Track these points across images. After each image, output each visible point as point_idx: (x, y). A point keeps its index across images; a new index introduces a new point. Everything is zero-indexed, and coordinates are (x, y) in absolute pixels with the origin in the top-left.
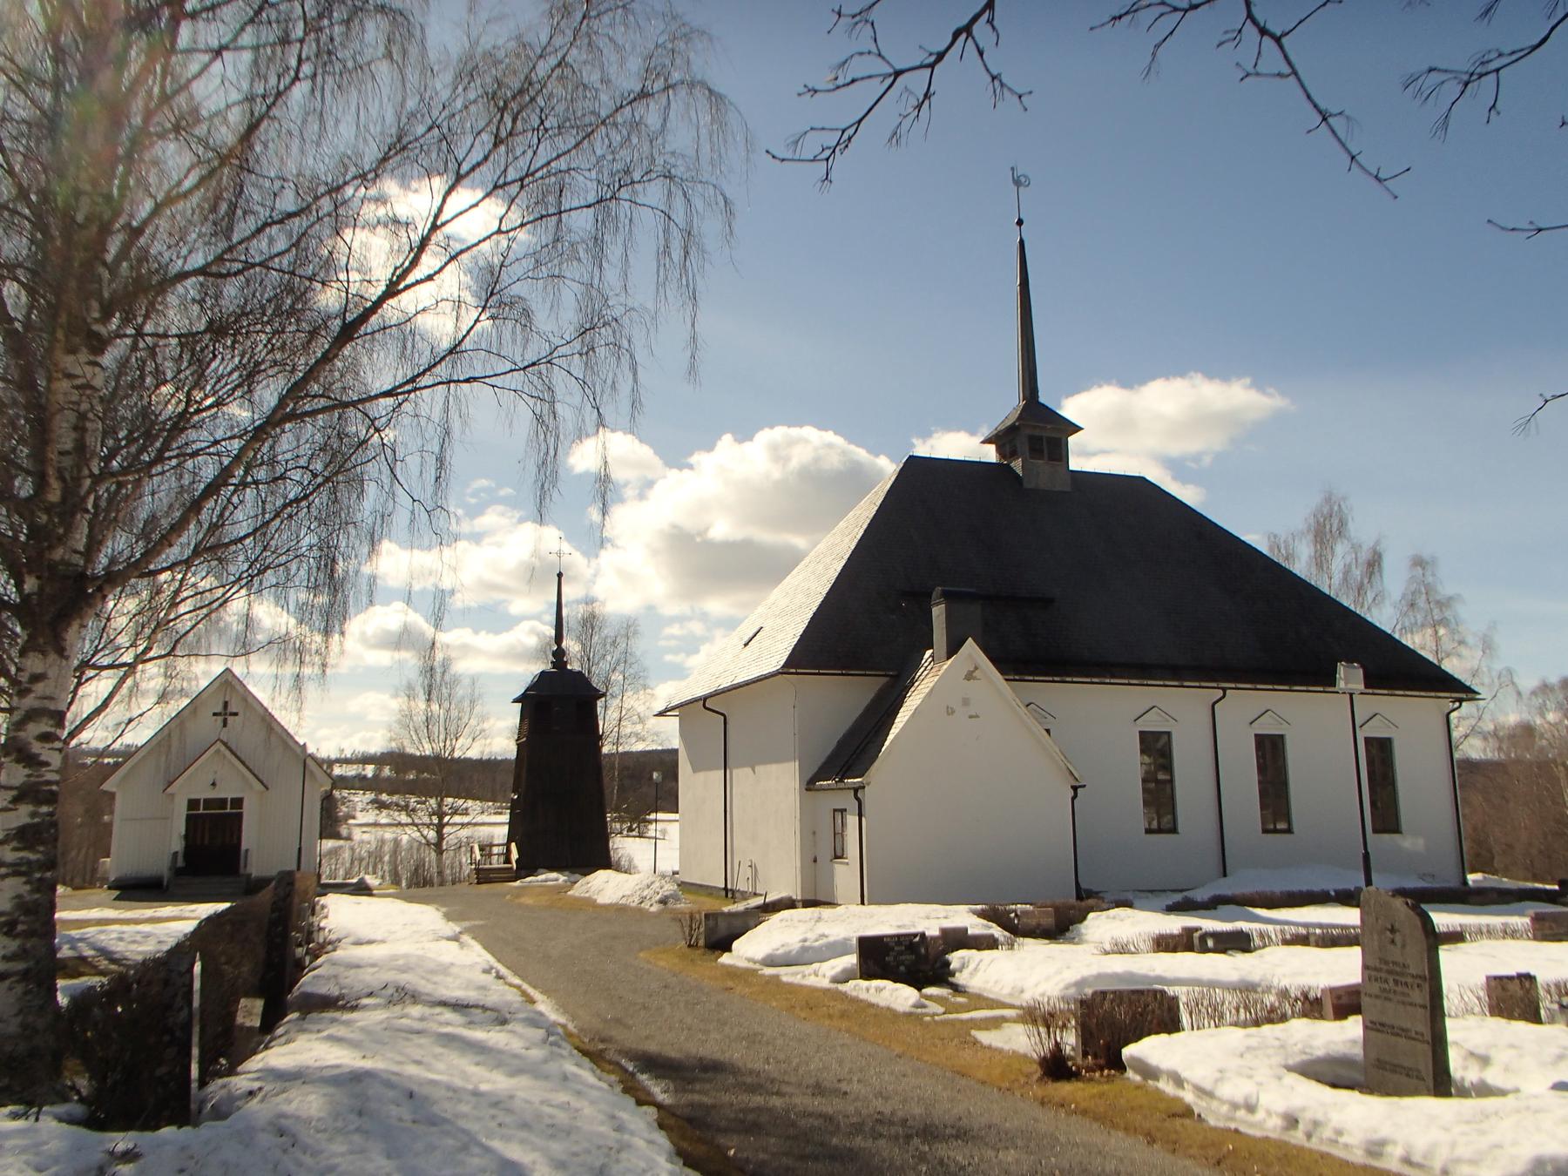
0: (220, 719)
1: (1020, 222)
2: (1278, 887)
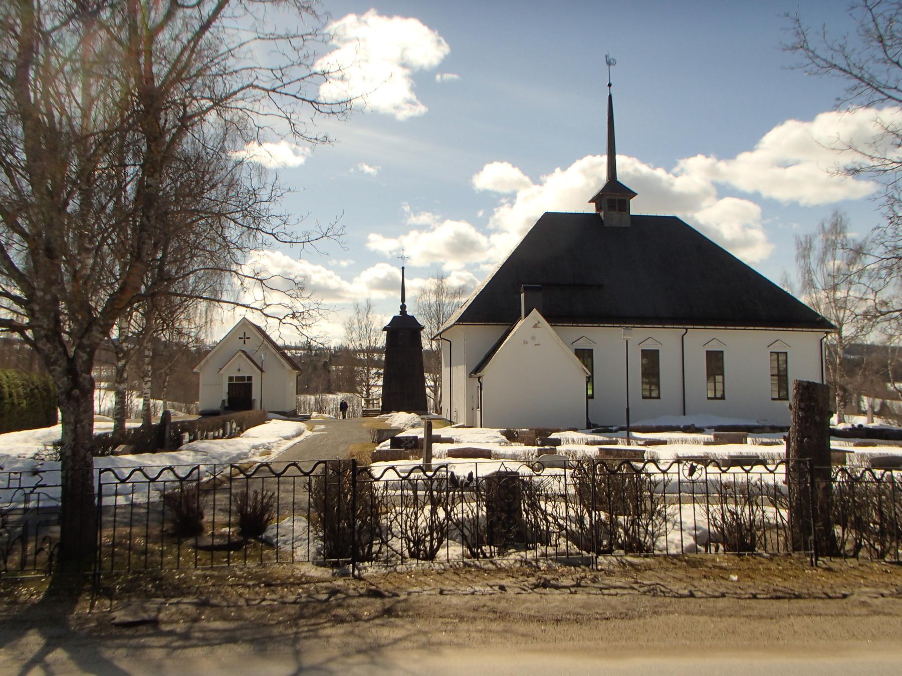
1: (610, 85)
2: (654, 424)
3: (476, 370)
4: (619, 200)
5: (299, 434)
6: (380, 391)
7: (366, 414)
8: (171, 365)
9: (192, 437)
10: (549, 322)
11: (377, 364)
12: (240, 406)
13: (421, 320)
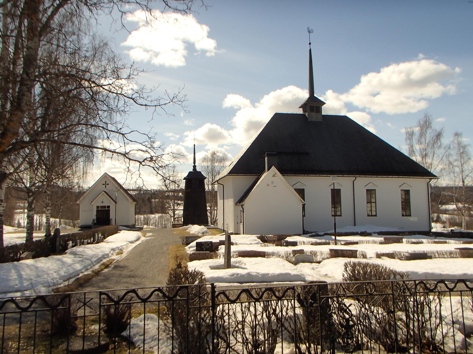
0: (104, 186)
1: (310, 44)
3: (240, 201)
4: (316, 107)
5: (138, 239)
6: (182, 213)
7: (174, 226)
8: (64, 201)
9: (74, 244)
10: (281, 174)
11: (180, 198)
12: (103, 223)
13: (204, 174)
